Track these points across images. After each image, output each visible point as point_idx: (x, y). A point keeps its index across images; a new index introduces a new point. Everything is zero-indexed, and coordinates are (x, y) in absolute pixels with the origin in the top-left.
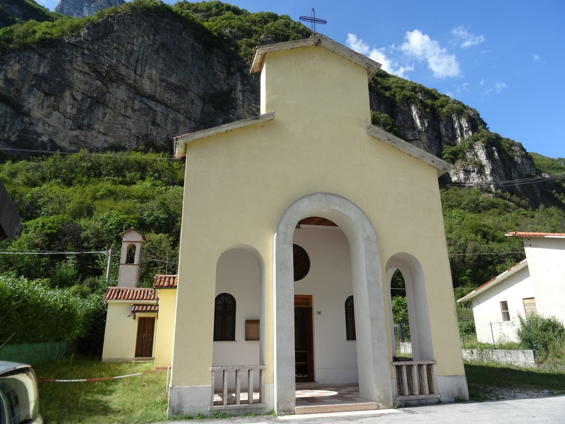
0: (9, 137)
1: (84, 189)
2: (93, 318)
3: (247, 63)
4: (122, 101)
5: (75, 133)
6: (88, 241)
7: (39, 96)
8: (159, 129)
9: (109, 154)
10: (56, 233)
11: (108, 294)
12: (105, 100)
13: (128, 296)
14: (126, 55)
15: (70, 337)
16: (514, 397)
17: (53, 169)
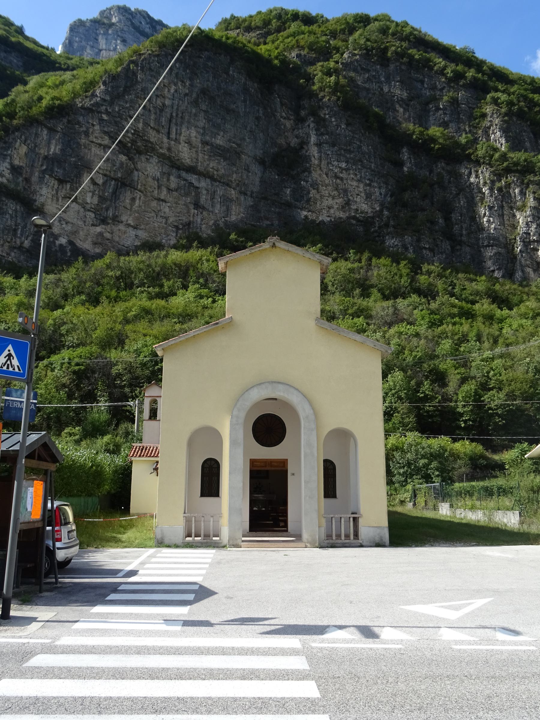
0: (22, 243)
1: (114, 309)
2: (122, 474)
3: (324, 100)
4: (154, 179)
5: (98, 229)
6: (121, 379)
7: (52, 184)
8: (204, 213)
9: (142, 256)
10: (85, 370)
11: (133, 452)
12: (132, 180)
13: (151, 454)
14: (156, 113)
15: (101, 493)
16: (439, 546)
17: (75, 283)
